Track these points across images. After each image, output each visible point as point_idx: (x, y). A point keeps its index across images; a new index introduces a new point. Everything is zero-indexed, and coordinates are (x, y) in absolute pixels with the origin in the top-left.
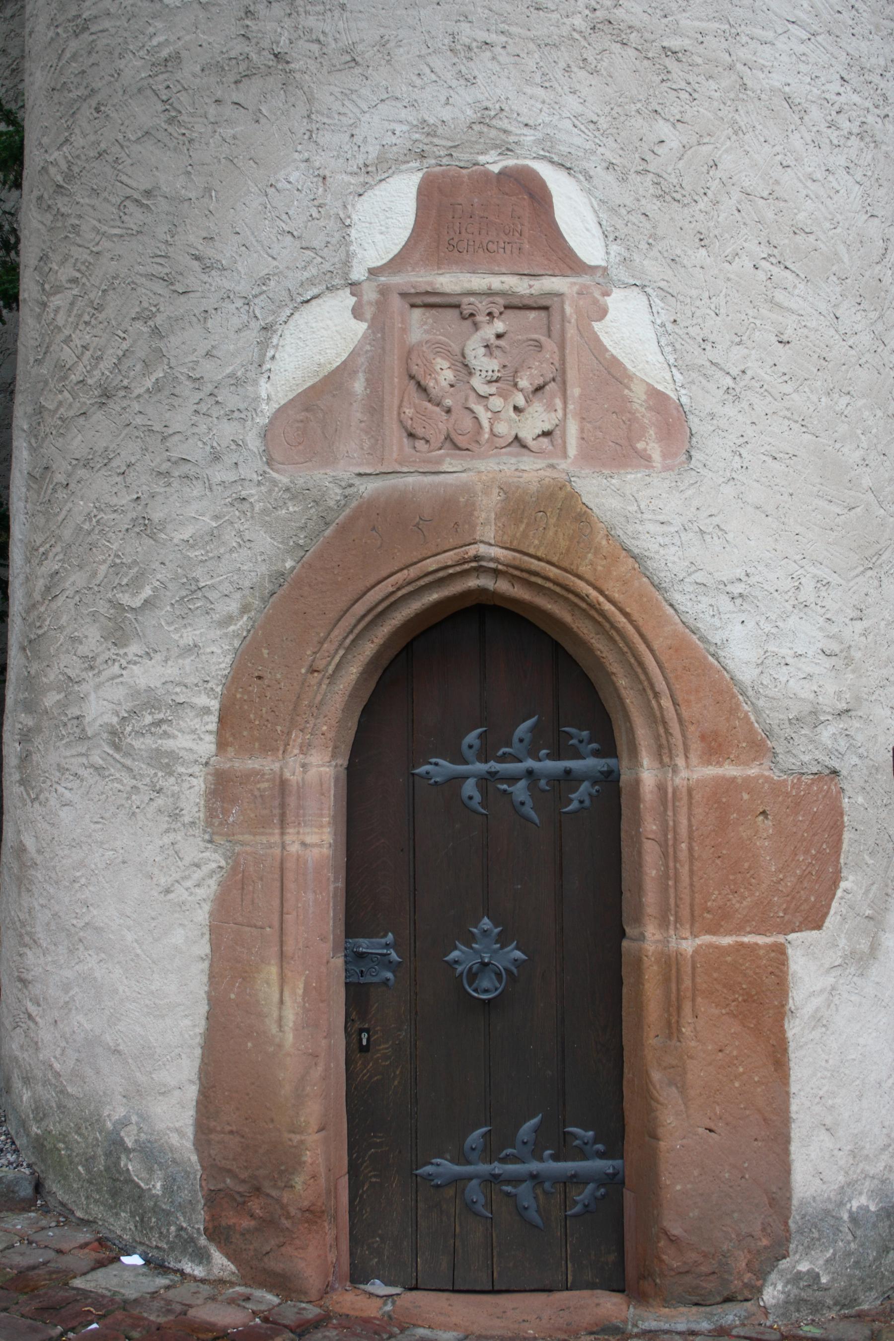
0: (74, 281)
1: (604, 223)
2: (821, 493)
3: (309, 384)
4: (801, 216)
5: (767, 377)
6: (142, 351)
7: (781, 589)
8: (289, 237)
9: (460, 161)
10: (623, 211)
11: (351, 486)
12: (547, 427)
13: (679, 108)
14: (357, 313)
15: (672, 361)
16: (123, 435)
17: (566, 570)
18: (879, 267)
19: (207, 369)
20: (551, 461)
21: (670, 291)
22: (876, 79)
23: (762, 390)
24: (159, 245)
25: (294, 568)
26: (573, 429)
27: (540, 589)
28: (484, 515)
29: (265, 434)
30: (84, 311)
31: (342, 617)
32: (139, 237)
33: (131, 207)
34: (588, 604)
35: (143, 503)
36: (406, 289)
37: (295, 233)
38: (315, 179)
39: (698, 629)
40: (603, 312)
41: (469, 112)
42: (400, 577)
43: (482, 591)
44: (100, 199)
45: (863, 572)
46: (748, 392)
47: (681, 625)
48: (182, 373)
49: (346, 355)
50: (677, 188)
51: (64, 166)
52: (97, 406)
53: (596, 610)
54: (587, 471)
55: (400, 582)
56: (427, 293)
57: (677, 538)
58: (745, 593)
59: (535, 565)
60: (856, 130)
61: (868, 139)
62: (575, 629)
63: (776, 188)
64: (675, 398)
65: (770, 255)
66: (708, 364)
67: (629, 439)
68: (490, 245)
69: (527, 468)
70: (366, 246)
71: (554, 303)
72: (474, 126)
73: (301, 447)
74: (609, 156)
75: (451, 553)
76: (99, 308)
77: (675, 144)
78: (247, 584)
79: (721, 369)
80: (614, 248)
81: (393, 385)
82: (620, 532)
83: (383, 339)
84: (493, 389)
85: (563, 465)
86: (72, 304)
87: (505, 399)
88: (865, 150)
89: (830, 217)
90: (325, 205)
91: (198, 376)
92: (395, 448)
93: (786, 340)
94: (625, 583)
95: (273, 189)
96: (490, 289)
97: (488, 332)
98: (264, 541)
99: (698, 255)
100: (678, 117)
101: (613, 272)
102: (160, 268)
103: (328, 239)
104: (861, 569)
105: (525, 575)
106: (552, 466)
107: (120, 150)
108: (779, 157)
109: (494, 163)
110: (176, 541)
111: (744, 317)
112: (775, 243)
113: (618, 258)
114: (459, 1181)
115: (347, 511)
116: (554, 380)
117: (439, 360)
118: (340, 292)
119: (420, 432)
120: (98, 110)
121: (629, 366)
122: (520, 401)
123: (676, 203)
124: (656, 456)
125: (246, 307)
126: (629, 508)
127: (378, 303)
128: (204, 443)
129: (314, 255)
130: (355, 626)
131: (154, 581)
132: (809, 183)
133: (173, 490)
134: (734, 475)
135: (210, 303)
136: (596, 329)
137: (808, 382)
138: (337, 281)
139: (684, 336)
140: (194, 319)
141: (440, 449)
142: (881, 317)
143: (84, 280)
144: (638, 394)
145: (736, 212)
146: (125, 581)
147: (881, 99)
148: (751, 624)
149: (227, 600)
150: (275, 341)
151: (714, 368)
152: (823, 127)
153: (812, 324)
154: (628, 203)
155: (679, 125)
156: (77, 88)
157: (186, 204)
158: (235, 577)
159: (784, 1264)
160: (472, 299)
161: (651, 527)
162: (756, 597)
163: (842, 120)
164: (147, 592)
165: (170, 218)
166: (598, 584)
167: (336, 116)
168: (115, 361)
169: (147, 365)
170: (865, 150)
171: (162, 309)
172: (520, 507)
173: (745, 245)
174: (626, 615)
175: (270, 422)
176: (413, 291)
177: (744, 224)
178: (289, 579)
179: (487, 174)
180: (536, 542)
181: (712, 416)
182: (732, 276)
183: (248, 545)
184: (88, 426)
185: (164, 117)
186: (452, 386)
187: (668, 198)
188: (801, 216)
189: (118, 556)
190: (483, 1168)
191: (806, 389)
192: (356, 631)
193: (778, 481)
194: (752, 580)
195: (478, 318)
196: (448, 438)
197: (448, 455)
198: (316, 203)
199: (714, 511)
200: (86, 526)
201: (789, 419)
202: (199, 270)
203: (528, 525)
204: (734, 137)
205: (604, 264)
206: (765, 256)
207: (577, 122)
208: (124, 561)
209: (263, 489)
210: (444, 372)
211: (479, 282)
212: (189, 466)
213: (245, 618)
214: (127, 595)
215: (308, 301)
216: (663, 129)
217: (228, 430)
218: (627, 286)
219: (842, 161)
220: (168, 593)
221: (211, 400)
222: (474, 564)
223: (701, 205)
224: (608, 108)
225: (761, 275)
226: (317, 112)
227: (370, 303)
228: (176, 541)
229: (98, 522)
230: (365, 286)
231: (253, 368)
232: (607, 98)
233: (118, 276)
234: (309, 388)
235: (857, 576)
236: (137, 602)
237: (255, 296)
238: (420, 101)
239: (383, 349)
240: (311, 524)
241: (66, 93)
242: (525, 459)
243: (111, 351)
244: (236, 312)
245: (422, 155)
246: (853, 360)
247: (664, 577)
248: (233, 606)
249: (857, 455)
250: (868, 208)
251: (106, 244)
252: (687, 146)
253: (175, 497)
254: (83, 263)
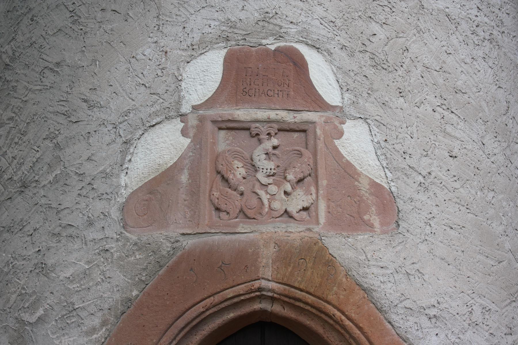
0: (11, 119)
1: (340, 80)
2: (481, 251)
3: (152, 177)
4: (459, 83)
5: (444, 177)
6: (48, 158)
7: (460, 313)
8: (143, 88)
9: (251, 42)
10: (352, 74)
11: (177, 241)
12: (306, 205)
13: (384, 16)
14: (184, 133)
15: (385, 165)
16: (33, 210)
17: (319, 298)
18: (505, 117)
19: (88, 168)
20: (309, 226)
21: (383, 122)
22: (497, 11)
23: (441, 185)
24: (63, 94)
25: (138, 295)
26: (322, 206)
27: (302, 310)
28: (264, 261)
29: (123, 209)
30: (15, 136)
31: (169, 328)
32: (51, 90)
33: (47, 72)
34: (334, 321)
35: (42, 253)
36: (216, 118)
37: (147, 85)
38: (161, 53)
39: (408, 339)
40: (341, 134)
41: (256, 15)
42: (208, 302)
43: (263, 312)
44: (30, 70)
45: (510, 303)
46: (433, 186)
47: (397, 336)
48: (72, 171)
49: (177, 159)
50: (385, 62)
51: (10, 53)
52: (18, 193)
53: (340, 325)
54: (332, 233)
55: (208, 305)
56: (229, 121)
57: (392, 277)
58: (438, 315)
59: (299, 294)
60: (487, 37)
61: (494, 43)
62: (326, 338)
63: (444, 65)
64: (388, 188)
65: (442, 104)
66: (408, 167)
67: (359, 213)
68: (269, 92)
69: (293, 231)
70: (191, 92)
71: (309, 127)
72: (259, 23)
73: (145, 217)
74: (342, 41)
75: (243, 286)
76: (24, 134)
77: (382, 37)
78: (107, 306)
79: (416, 171)
80: (347, 95)
81: (205, 181)
82: (355, 273)
83: (201, 149)
84: (271, 180)
85: (316, 229)
86: (9, 133)
87: (279, 187)
88: (493, 49)
89: (476, 85)
90: (166, 68)
91: (82, 173)
92: (207, 217)
93: (454, 155)
94: (359, 307)
95: (134, 59)
96: (269, 119)
97: (268, 145)
98: (119, 278)
99: (399, 101)
100: (384, 21)
101: (346, 110)
102: (62, 108)
103: (168, 88)
104: (509, 301)
105: (292, 301)
106: (309, 230)
107: (43, 41)
108: (445, 48)
109: (272, 44)
110: (61, 278)
111: (428, 140)
112: (445, 97)
113: (349, 102)
115: (175, 258)
116: (310, 175)
117: (236, 162)
118: (174, 120)
119: (223, 207)
120: (32, 20)
121: (358, 167)
122: (288, 188)
123: (384, 71)
124: (377, 224)
125: (115, 130)
126: (360, 257)
127: (197, 126)
128: (83, 215)
129: (158, 98)
130: (177, 335)
131: (45, 305)
132: (463, 64)
133: (62, 245)
134: (427, 238)
135: (91, 128)
136: (336, 144)
137: (469, 182)
138: (172, 113)
139: (392, 150)
140: (82, 138)
141: (236, 218)
142: (508, 146)
143: (17, 118)
144: (364, 186)
145: (421, 78)
146: (27, 305)
147: (500, 22)
148: (442, 336)
149: (93, 317)
150: (131, 150)
151: (411, 170)
152: (469, 33)
153: (470, 147)
154: (355, 69)
155: (384, 26)
156: (21, 9)
157: (81, 69)
158: (99, 302)
160: (257, 125)
161: (375, 270)
162: (445, 318)
163: (479, 30)
164: (41, 312)
165: (70, 78)
166: (341, 307)
167: (175, 17)
168: (31, 165)
169: (50, 167)
170: (493, 49)
171: (62, 132)
172: (290, 256)
173: (427, 97)
174: (360, 329)
175: (126, 201)
176: (220, 119)
177: (426, 85)
178: (134, 304)
179: (267, 51)
180: (299, 279)
181: (411, 200)
182: (420, 115)
183: (108, 280)
184: (13, 206)
185: (70, 20)
186: (244, 178)
187: (379, 67)
188: (459, 83)
189: (23, 288)
191: (468, 186)
192: (178, 339)
193: (454, 242)
194: (442, 306)
195: (261, 137)
196: (241, 211)
197: (241, 222)
198: (160, 67)
199: (415, 261)
200: (6, 270)
201: (459, 204)
202: (87, 108)
203: (294, 268)
204: (417, 35)
205: (340, 105)
206: (439, 104)
207: (322, 22)
208: (27, 291)
209: (120, 243)
210: (239, 169)
211: (261, 114)
212: (73, 229)
213: (104, 330)
214: (27, 314)
215: (153, 126)
216: (375, 28)
217: (99, 206)
218: (355, 118)
219: (480, 53)
220: (54, 313)
221: (90, 187)
222: (258, 293)
223: (400, 72)
224: (342, 14)
225: (437, 116)
226: (163, 14)
227: (193, 127)
228: (61, 278)
229: (13, 266)
230: (190, 116)
231: (116, 167)
232: (341, 9)
233: (37, 114)
234: (152, 179)
235: (507, 306)
236: (33, 319)
237: (120, 123)
238: (226, 8)
239: (201, 155)
240: (150, 267)
241: (15, 13)
242: (292, 225)
243: (30, 159)
244: (108, 132)
245: (227, 39)
246: (495, 170)
247: (384, 303)
248: (96, 321)
249: (501, 228)
250: (497, 82)
251: (31, 95)
252: (390, 38)
253: (63, 249)
254: (17, 108)
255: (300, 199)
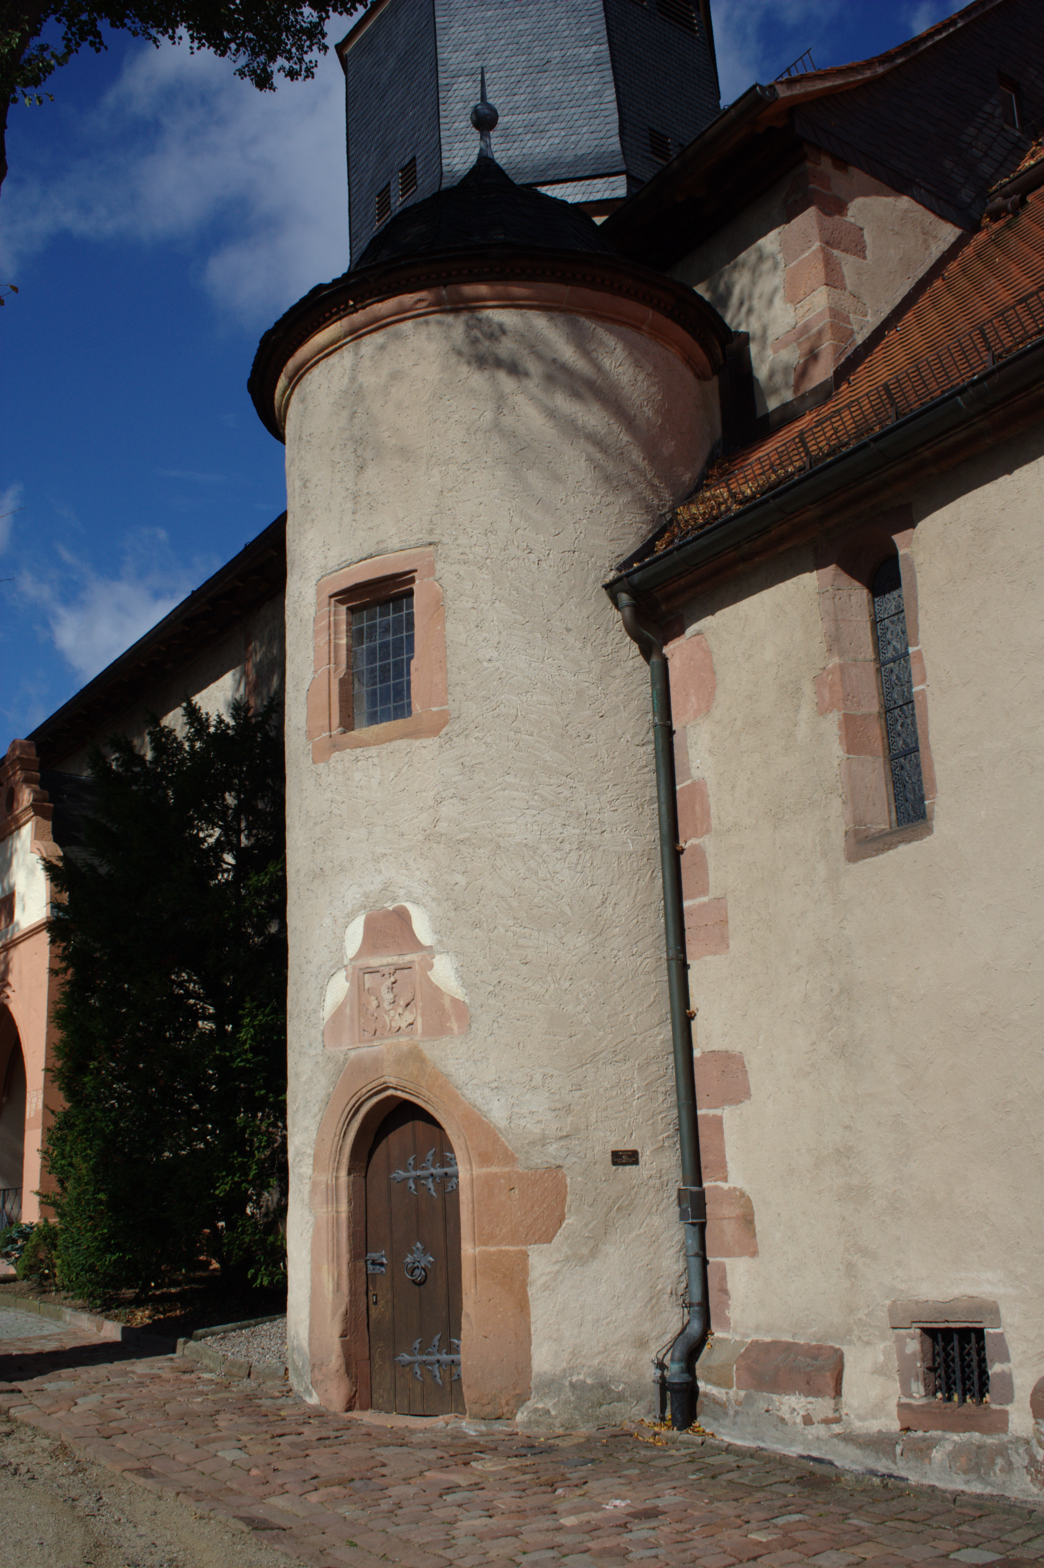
12: (410, 1021)
26: (419, 1021)
40: (431, 967)
109: (390, 906)
114: (410, 1364)
148: (503, 1100)
159: (528, 1403)
190: (419, 1358)
245: (365, 907)
255: (408, 1017)
